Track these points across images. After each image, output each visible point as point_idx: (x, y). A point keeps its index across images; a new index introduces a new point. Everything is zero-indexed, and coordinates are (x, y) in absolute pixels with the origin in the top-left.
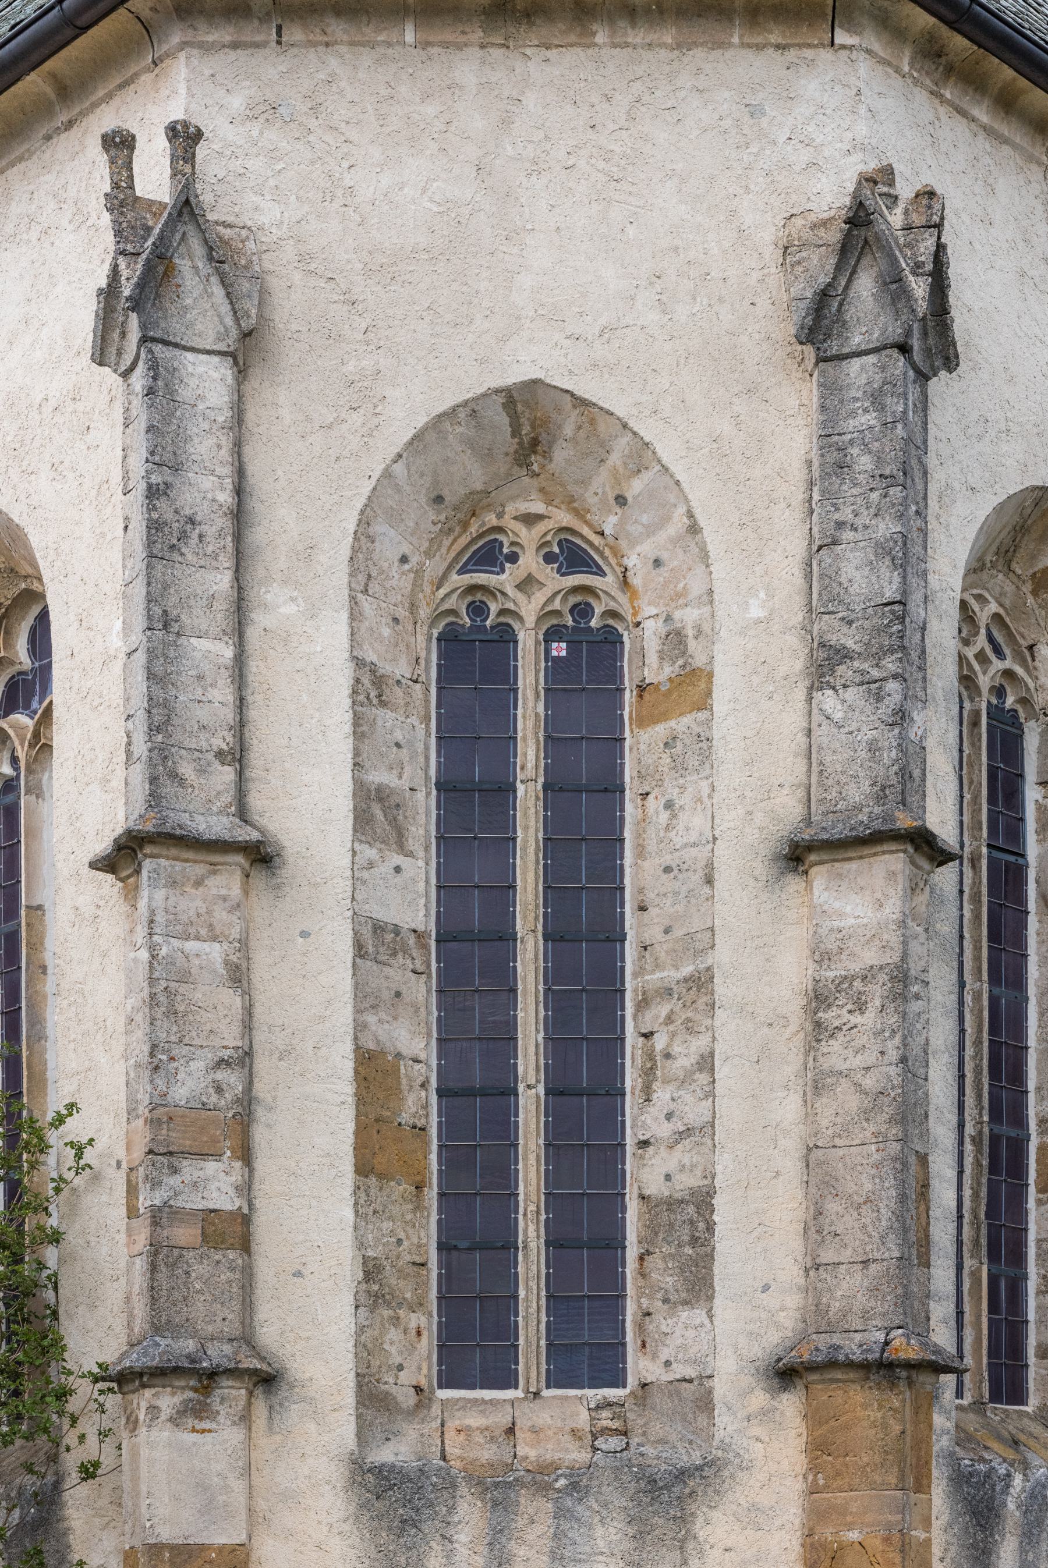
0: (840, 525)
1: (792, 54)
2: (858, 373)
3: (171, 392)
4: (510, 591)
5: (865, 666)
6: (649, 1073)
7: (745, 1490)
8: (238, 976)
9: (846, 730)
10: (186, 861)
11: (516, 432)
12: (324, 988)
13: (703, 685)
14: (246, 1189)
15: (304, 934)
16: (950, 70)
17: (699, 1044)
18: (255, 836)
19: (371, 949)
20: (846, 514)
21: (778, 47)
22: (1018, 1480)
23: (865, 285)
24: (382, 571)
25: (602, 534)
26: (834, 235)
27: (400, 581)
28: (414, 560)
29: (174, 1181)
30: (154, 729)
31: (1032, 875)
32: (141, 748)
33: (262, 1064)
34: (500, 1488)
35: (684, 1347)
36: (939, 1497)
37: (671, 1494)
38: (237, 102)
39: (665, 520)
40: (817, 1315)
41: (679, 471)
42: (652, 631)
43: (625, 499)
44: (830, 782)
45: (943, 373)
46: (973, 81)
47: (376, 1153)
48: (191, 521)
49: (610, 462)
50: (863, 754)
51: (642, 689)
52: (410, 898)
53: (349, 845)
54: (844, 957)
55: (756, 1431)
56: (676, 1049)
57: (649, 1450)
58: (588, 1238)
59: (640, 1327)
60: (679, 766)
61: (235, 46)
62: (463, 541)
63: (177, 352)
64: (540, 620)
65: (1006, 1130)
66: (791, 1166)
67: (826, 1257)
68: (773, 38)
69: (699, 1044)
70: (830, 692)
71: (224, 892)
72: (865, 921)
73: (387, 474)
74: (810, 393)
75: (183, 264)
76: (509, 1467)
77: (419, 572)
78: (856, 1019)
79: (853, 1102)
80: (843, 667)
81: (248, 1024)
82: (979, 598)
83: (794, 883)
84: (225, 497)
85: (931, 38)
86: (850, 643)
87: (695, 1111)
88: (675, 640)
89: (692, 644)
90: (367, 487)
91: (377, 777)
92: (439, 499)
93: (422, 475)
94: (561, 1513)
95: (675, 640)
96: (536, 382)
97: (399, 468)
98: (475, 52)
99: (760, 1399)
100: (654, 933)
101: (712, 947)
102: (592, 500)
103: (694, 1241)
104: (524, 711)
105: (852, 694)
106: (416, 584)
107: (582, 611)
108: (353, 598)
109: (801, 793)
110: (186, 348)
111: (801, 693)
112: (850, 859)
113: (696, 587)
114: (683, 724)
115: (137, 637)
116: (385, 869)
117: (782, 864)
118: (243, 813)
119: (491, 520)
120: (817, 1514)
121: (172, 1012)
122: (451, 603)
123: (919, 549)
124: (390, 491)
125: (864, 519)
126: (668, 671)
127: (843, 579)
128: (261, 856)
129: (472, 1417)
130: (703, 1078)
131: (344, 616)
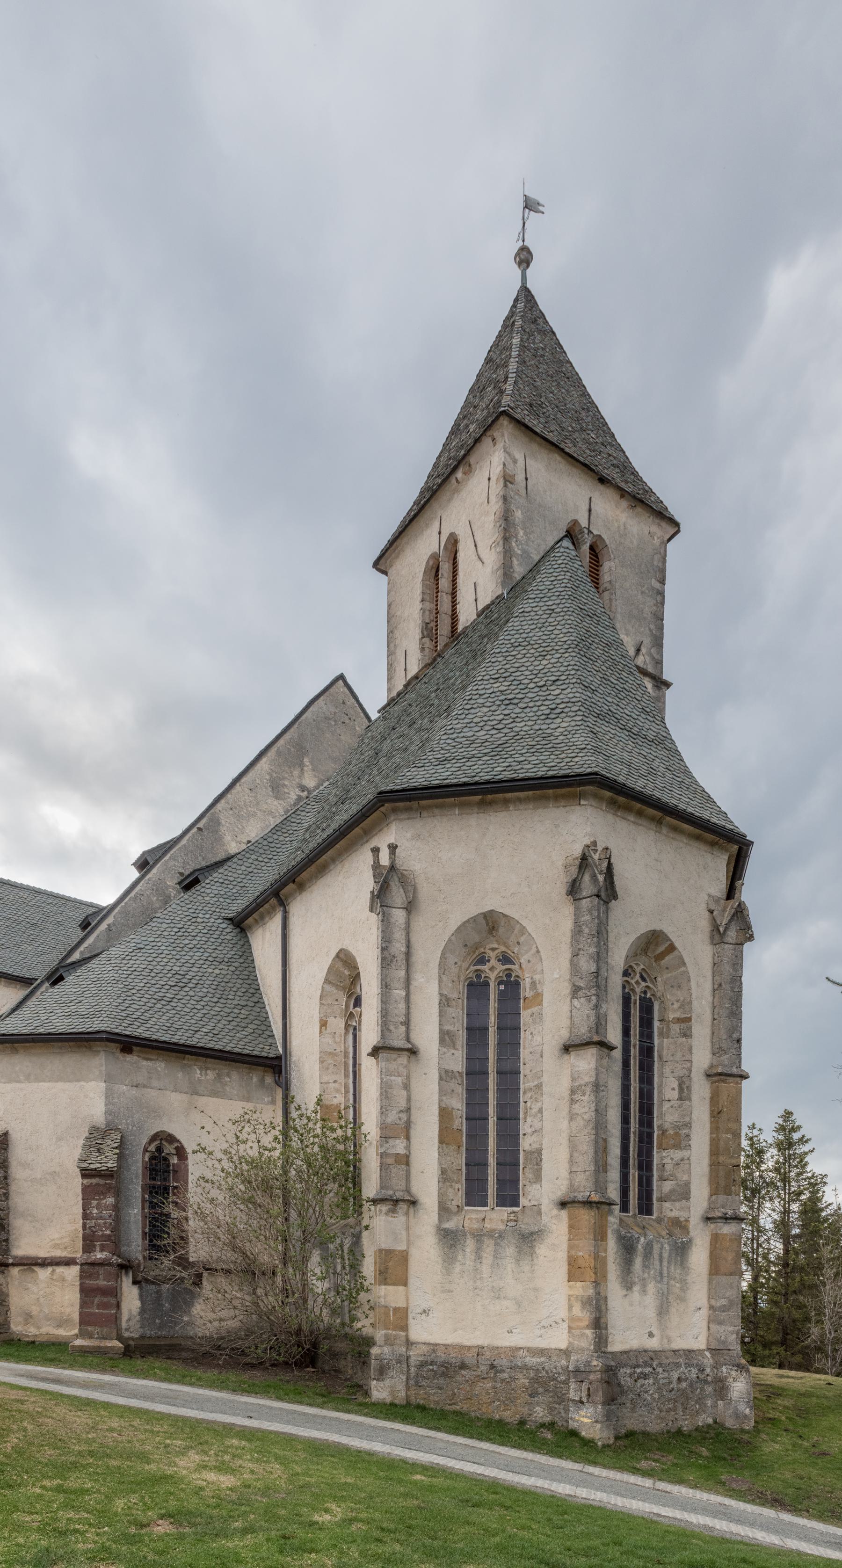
0: (579, 949)
1: (568, 808)
2: (585, 903)
3: (389, 922)
4: (487, 971)
6: (526, 1113)
7: (550, 1240)
8: (407, 1087)
11: (488, 924)
12: (431, 1090)
14: (408, 1148)
15: (425, 1074)
16: (619, 807)
17: (539, 1105)
18: (410, 1046)
20: (581, 946)
22: (642, 1239)
23: (587, 878)
26: (577, 862)
27: (454, 970)
28: (459, 963)
29: (387, 1145)
30: (383, 1017)
31: (656, 1049)
32: (380, 1022)
33: (413, 1111)
34: (479, 1236)
35: (534, 1196)
36: (612, 1244)
37: (528, 1240)
38: (409, 835)
39: (531, 949)
40: (571, 1187)
41: (533, 934)
42: (528, 981)
45: (613, 901)
46: (628, 809)
47: (445, 1137)
48: (394, 956)
50: (585, 1018)
51: (525, 999)
52: (457, 1061)
55: (554, 1221)
56: (533, 1106)
57: (523, 1226)
58: (509, 1163)
59: (523, 1190)
60: (534, 1022)
61: (408, 819)
62: (474, 956)
64: (496, 979)
65: (646, 1130)
66: (565, 1142)
67: (574, 1169)
68: (562, 804)
69: (539, 1105)
73: (450, 940)
74: (572, 909)
75: (392, 884)
76: (482, 1230)
77: (460, 967)
78: (583, 1098)
79: (582, 1123)
81: (409, 1100)
82: (637, 964)
83: (566, 1057)
84: (403, 949)
85: (612, 798)
87: (537, 1125)
88: (533, 984)
89: (538, 985)
90: (444, 944)
91: (447, 1027)
92: (466, 945)
94: (497, 1244)
95: (533, 984)
97: (453, 938)
98: (476, 815)
99: (555, 1212)
100: (527, 1072)
103: (537, 1164)
104: (491, 1005)
105: (582, 1000)
106: (460, 970)
107: (509, 976)
108: (440, 977)
109: (568, 1030)
111: (568, 1000)
113: (539, 969)
114: (535, 1009)
115: (379, 991)
116: (449, 1054)
118: (408, 1040)
119: (482, 950)
120: (570, 1247)
121: (387, 1097)
122: (470, 975)
123: (605, 955)
125: (586, 947)
126: (532, 993)
128: (413, 1052)
129: (473, 1216)
130: (539, 1115)
131: (437, 981)
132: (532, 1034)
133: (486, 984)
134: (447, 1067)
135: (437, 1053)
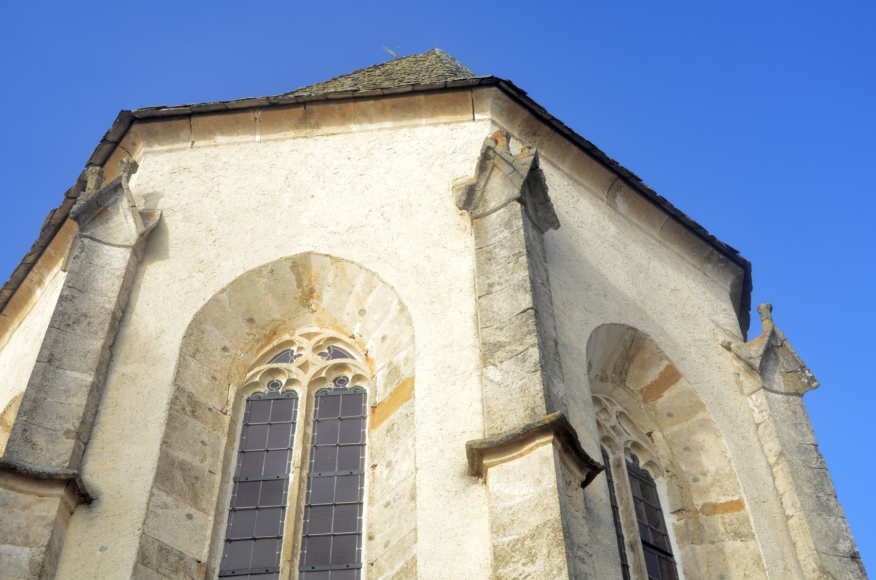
5: (514, 347)
9: (505, 384)
10: (20, 491)
11: (300, 285)
13: (409, 386)
19: (154, 562)
20: (495, 279)
21: (445, 123)
24: (207, 350)
25: (353, 337)
43: (364, 310)
44: (496, 417)
49: (354, 292)
53: (149, 488)
54: (515, 526)
63: (99, 244)
64: (311, 384)
70: (492, 367)
71: (43, 514)
72: (529, 496)
74: (470, 241)
78: (530, 568)
80: (500, 352)
86: (502, 339)
88: (394, 371)
91: (181, 455)
93: (240, 304)
95: (394, 371)
96: (309, 253)
97: (224, 296)
101: (416, 542)
102: (346, 318)
110: (104, 243)
112: (514, 458)
117: (466, 480)
119: (286, 337)
124: (217, 309)
127: (496, 309)
128: (81, 495)
132: (389, 464)
133: (290, 398)
134: (166, 539)
135: (145, 499)
